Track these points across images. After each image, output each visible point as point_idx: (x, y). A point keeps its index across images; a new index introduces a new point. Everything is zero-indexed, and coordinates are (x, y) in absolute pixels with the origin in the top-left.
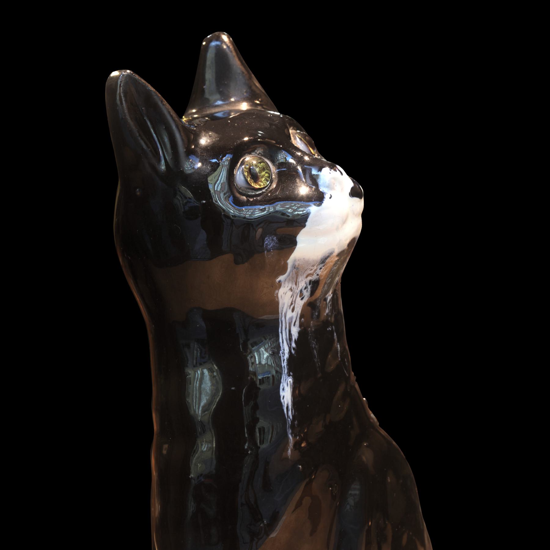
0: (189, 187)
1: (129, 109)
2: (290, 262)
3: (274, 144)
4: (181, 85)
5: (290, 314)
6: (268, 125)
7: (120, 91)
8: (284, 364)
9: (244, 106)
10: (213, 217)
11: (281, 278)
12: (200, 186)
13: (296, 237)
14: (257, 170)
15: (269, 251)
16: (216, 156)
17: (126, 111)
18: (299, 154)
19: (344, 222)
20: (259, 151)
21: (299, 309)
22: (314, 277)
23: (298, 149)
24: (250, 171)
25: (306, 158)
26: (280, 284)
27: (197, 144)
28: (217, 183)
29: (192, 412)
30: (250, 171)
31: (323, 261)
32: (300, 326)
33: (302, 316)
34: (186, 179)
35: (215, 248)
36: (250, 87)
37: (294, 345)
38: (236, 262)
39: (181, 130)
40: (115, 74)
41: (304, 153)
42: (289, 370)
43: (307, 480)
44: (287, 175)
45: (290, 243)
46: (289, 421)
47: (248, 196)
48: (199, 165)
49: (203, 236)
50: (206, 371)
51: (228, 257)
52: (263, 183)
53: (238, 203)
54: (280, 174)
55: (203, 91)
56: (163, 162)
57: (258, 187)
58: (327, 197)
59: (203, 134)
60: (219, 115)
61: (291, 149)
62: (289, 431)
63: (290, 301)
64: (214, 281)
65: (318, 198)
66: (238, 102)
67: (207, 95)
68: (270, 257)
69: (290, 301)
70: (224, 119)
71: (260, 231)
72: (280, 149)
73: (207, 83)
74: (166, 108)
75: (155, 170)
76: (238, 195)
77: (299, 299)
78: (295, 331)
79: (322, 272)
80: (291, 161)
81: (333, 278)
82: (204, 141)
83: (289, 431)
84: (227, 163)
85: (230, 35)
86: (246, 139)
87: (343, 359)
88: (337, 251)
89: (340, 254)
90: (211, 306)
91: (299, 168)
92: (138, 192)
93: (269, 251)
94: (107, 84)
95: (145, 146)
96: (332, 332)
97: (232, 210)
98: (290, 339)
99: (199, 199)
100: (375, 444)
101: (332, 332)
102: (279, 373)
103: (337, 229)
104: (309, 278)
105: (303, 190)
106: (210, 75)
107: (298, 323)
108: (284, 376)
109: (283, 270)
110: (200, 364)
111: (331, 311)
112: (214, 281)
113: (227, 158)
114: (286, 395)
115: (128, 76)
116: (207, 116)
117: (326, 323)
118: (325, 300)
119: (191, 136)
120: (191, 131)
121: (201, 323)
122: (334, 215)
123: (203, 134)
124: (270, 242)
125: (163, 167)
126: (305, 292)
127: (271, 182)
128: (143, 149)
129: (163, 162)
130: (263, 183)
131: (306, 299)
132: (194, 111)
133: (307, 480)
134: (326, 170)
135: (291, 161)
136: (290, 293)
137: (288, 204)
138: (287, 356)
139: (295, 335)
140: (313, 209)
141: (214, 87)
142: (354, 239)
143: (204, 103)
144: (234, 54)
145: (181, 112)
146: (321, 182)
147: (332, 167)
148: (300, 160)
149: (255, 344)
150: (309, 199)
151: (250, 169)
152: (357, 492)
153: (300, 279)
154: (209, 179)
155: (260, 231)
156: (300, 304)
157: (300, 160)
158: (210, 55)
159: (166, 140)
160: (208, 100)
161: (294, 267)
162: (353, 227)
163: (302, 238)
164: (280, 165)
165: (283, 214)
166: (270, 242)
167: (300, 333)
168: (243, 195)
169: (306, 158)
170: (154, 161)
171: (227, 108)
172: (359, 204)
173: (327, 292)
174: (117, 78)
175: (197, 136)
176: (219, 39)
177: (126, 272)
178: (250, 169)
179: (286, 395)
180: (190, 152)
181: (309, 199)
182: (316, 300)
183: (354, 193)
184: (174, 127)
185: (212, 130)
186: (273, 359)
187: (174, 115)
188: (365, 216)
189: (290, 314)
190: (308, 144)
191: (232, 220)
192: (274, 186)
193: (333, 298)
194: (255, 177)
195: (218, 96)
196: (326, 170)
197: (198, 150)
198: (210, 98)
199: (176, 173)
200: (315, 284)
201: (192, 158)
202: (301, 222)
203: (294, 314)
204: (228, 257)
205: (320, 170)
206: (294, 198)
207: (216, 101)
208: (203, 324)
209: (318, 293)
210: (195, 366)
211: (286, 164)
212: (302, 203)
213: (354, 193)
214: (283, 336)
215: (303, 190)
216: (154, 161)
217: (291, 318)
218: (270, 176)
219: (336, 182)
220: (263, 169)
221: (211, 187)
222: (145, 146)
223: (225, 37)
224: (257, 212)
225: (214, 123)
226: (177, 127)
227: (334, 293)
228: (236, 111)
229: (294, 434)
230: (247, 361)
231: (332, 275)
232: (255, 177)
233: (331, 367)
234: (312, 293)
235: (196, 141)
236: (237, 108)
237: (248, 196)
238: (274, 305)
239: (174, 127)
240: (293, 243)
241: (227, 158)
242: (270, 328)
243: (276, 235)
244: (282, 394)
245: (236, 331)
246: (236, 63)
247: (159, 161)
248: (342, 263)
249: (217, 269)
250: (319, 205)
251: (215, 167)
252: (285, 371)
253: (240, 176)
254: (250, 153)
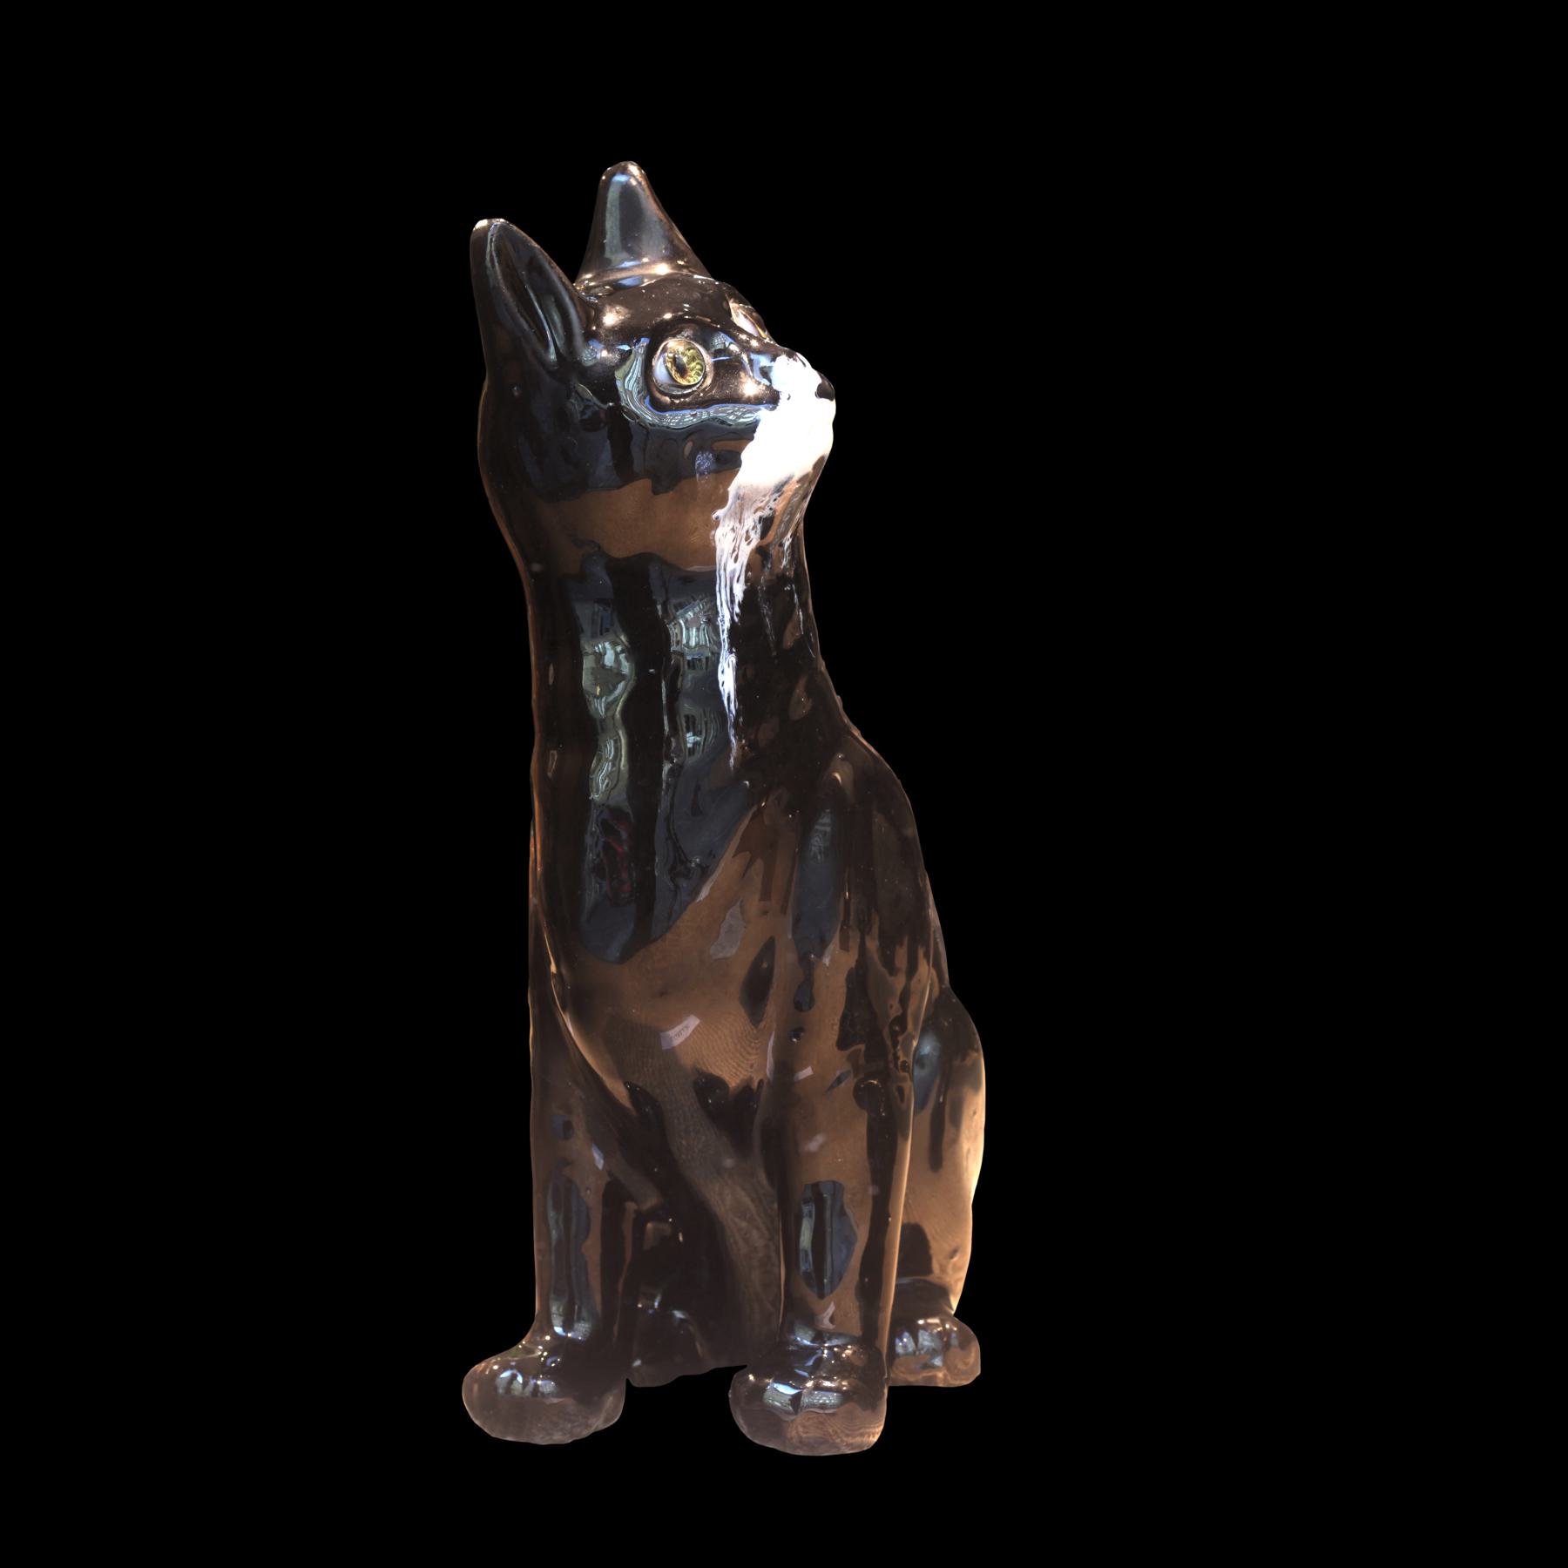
0: (589, 385)
2: (732, 490)
3: (708, 324)
4: (572, 238)
5: (731, 566)
6: (697, 295)
7: (490, 248)
8: (724, 636)
9: (663, 269)
11: (720, 513)
12: (605, 384)
13: (739, 454)
14: (685, 360)
15: (702, 474)
16: (627, 341)
18: (744, 337)
20: (688, 333)
21: (744, 559)
22: (766, 513)
23: (742, 331)
24: (674, 360)
25: (754, 343)
26: (717, 523)
27: (600, 324)
28: (629, 382)
30: (674, 360)
31: (779, 489)
32: (747, 580)
33: (749, 567)
34: (584, 373)
35: (624, 471)
36: (671, 242)
37: (737, 610)
38: (655, 492)
40: (482, 224)
42: (731, 645)
43: (755, 808)
44: (728, 368)
45: (729, 463)
47: (672, 397)
48: (604, 354)
49: (606, 457)
52: (693, 378)
53: (657, 406)
54: (717, 365)
55: (602, 247)
56: (552, 349)
57: (684, 383)
58: (783, 397)
60: (626, 282)
61: (731, 330)
62: (732, 732)
63: (732, 545)
64: (624, 517)
65: (772, 398)
67: (608, 255)
68: (703, 483)
69: (732, 545)
70: (636, 288)
71: (689, 447)
72: (717, 330)
73: (608, 236)
74: (555, 273)
75: (543, 363)
76: (658, 395)
77: (744, 543)
78: (739, 590)
79: (779, 505)
80: (734, 348)
81: (792, 515)
82: (611, 318)
83: (732, 732)
84: (641, 351)
85: (642, 166)
87: (807, 630)
88: (798, 475)
89: (801, 480)
90: (619, 551)
91: (744, 357)
92: (516, 391)
93: (702, 474)
94: (473, 237)
96: (791, 593)
97: (649, 416)
98: (732, 601)
99: (605, 402)
100: (853, 759)
101: (791, 593)
102: (717, 655)
104: (759, 514)
106: (612, 223)
107: (742, 578)
109: (722, 501)
110: (601, 632)
111: (790, 562)
112: (624, 517)
113: (644, 342)
115: (502, 226)
116: (609, 283)
117: (782, 579)
118: (781, 545)
119: (591, 315)
120: (590, 305)
122: (792, 427)
124: (704, 461)
125: (553, 357)
127: (705, 377)
128: (523, 331)
129: (552, 349)
130: (693, 378)
131: (754, 543)
132: (589, 276)
133: (755, 808)
134: (783, 359)
135: (734, 348)
137: (729, 407)
138: (727, 625)
139: (739, 596)
140: (763, 414)
141: (617, 241)
142: (822, 458)
143: (604, 265)
144: (648, 192)
145: (573, 275)
146: (773, 375)
147: (790, 356)
148: (745, 347)
149: (680, 606)
150: (757, 401)
151: (674, 359)
152: (828, 829)
153: (746, 514)
154: (618, 374)
155: (689, 447)
156: (746, 551)
157: (745, 347)
158: (613, 195)
159: (557, 318)
160: (609, 261)
161: (738, 497)
162: (822, 442)
163: (748, 454)
165: (723, 422)
166: (704, 461)
167: (745, 592)
168: (665, 394)
169: (754, 343)
170: (540, 348)
171: (638, 272)
172: (829, 408)
173: (784, 535)
174: (485, 230)
175: (599, 312)
176: (624, 171)
177: (443, 545)
178: (674, 359)
180: (590, 336)
181: (757, 401)
182: (769, 545)
183: (821, 393)
184: (567, 300)
185: (621, 304)
186: (708, 636)
187: (565, 279)
188: (837, 425)
189: (731, 566)
190: (756, 323)
191: (647, 430)
192: (709, 381)
193: (792, 544)
194: (682, 370)
195: (625, 255)
196: (783, 359)
197: (602, 331)
198: (613, 258)
200: (766, 523)
201: (594, 344)
202: (747, 433)
203: (738, 566)
204: (643, 485)
205: (774, 360)
206: (736, 399)
208: (606, 578)
209: (771, 534)
211: (725, 351)
212: (749, 407)
213: (821, 393)
214: (722, 597)
216: (540, 348)
217: (734, 571)
218: (703, 369)
219: (796, 377)
220: (693, 359)
221: (619, 384)
222: (526, 326)
223: (633, 169)
224: (687, 418)
225: (618, 293)
226: (572, 299)
227: (794, 536)
228: (651, 277)
230: (668, 636)
231: (790, 510)
232: (682, 370)
233: (789, 641)
234: (763, 535)
235: (597, 320)
237: (672, 397)
238: (709, 553)
239: (567, 300)
241: (644, 342)
242: (704, 584)
243: (712, 451)
244: (721, 678)
245: (653, 586)
246: (651, 206)
247: (547, 347)
248: (804, 497)
249: (631, 497)
251: (625, 356)
252: (726, 645)
253: (660, 370)
254: (674, 336)
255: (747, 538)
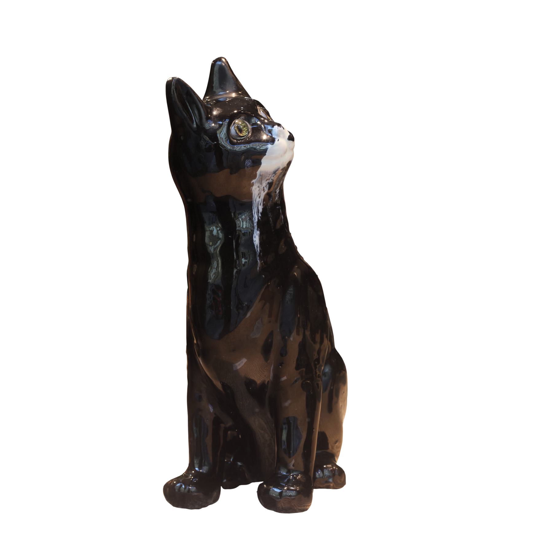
1: (178, 96)
2: (258, 173)
5: (258, 200)
8: (255, 224)
9: (234, 95)
10: (218, 149)
11: (254, 181)
12: (213, 136)
13: (261, 160)
14: (242, 127)
15: (248, 167)
17: (176, 98)
19: (285, 153)
20: (243, 117)
21: (262, 197)
22: (270, 181)
23: (262, 117)
24: (238, 127)
25: (266, 121)
26: (253, 184)
27: (211, 114)
28: (222, 135)
29: (209, 251)
30: (238, 127)
31: (275, 172)
34: (206, 131)
35: (220, 166)
37: (260, 215)
38: (231, 174)
39: (197, 101)
41: (265, 118)
42: (258, 227)
43: (266, 285)
45: (257, 163)
46: (258, 253)
47: (237, 140)
48: (213, 125)
49: (214, 161)
50: (214, 227)
51: (227, 171)
52: (244, 134)
53: (232, 143)
54: (253, 129)
56: (195, 123)
58: (276, 140)
59: (214, 109)
60: (221, 100)
62: (258, 258)
65: (272, 141)
66: (231, 93)
67: (214, 90)
68: (248, 170)
70: (225, 102)
73: (215, 83)
75: (191, 128)
76: (232, 139)
77: (262, 192)
78: (261, 208)
80: (259, 122)
82: (215, 113)
83: (258, 258)
84: (226, 124)
86: (236, 111)
88: (281, 168)
90: (218, 195)
92: (182, 138)
93: (248, 167)
95: (185, 115)
96: (279, 209)
97: (229, 147)
98: (258, 212)
99: (213, 142)
101: (279, 209)
102: (253, 231)
103: (282, 156)
104: (268, 181)
105: (265, 137)
107: (262, 204)
108: (255, 230)
109: (255, 177)
110: (212, 223)
111: (279, 198)
113: (227, 121)
114: (256, 240)
118: (276, 192)
121: (213, 204)
123: (214, 109)
124: (248, 163)
125: (195, 126)
126: (265, 188)
127: (249, 133)
129: (195, 123)
130: (244, 134)
131: (266, 191)
133: (266, 285)
135: (259, 122)
136: (258, 189)
137: (257, 144)
138: (256, 220)
139: (261, 210)
140: (269, 146)
141: (218, 85)
146: (273, 133)
148: (263, 122)
149: (240, 214)
150: (267, 141)
152: (292, 292)
153: (263, 181)
154: (218, 132)
156: (263, 194)
157: (263, 122)
160: (215, 92)
161: (260, 175)
164: (253, 124)
165: (255, 149)
166: (248, 163)
167: (263, 209)
169: (266, 121)
171: (225, 96)
173: (276, 189)
179: (256, 240)
180: (208, 119)
182: (271, 192)
184: (200, 106)
185: (219, 107)
189: (258, 200)
191: (229, 152)
192: (250, 134)
195: (220, 90)
198: (216, 91)
199: (201, 128)
200: (270, 185)
201: (209, 121)
202: (264, 153)
203: (260, 200)
204: (227, 171)
205: (273, 127)
206: (260, 141)
207: (220, 92)
209: (272, 188)
210: (209, 224)
212: (264, 144)
214: (255, 211)
215: (265, 137)
217: (259, 202)
218: (248, 130)
220: (244, 127)
221: (218, 135)
222: (185, 115)
224: (243, 147)
226: (202, 105)
228: (230, 98)
229: (261, 260)
232: (241, 131)
234: (269, 188)
235: (211, 113)
236: (230, 96)
237: (237, 140)
238: (250, 195)
239: (200, 106)
240: (260, 164)
241: (227, 121)
242: (248, 206)
243: (251, 159)
244: (254, 239)
247: (193, 122)
250: (273, 144)
251: (221, 126)
252: (256, 228)
253: (233, 130)
254: (238, 118)
255: (264, 190)
